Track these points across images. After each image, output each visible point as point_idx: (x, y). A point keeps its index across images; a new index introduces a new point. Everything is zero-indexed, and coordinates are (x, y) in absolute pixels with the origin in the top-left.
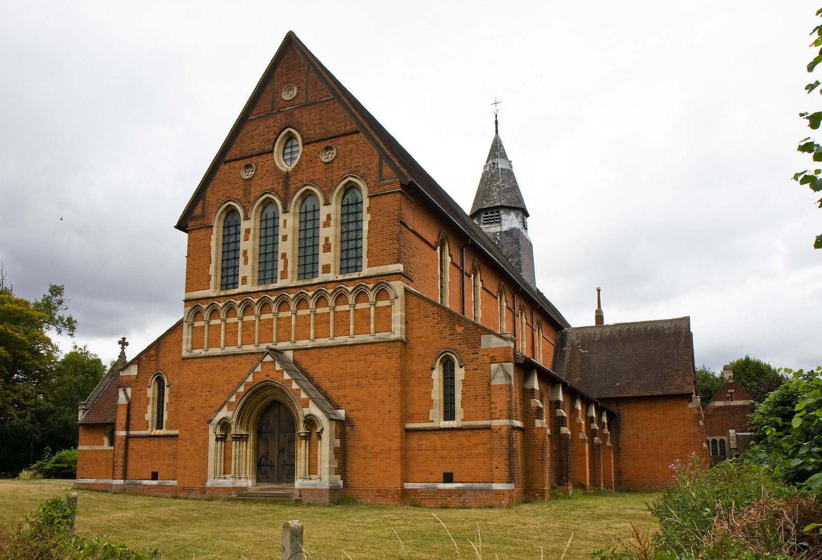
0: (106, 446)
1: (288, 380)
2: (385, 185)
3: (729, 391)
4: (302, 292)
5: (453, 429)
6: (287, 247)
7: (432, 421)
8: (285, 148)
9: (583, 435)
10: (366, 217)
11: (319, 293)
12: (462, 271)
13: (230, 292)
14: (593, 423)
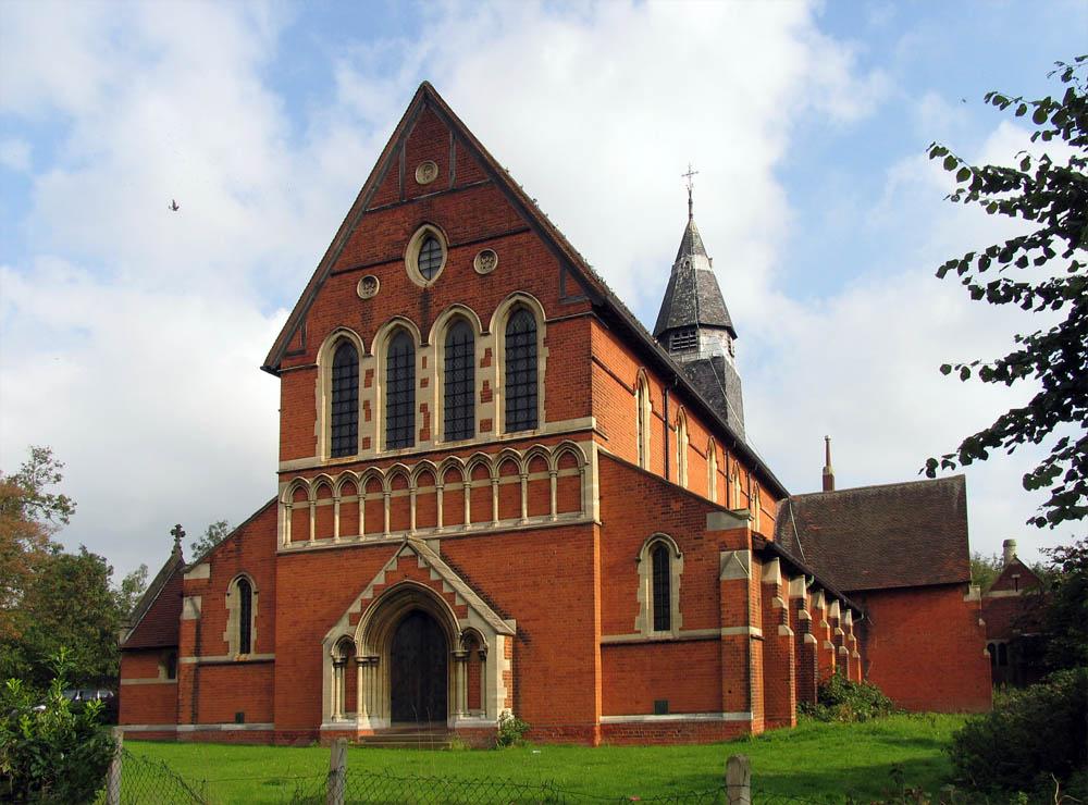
0: (162, 678)
1: (437, 581)
2: (568, 306)
3: (1014, 576)
4: (451, 459)
5: (668, 642)
6: (432, 395)
7: (639, 632)
8: (421, 253)
9: (829, 644)
10: (543, 353)
11: (475, 460)
12: (666, 422)
13: (345, 460)
14: (782, 623)
